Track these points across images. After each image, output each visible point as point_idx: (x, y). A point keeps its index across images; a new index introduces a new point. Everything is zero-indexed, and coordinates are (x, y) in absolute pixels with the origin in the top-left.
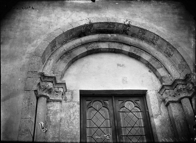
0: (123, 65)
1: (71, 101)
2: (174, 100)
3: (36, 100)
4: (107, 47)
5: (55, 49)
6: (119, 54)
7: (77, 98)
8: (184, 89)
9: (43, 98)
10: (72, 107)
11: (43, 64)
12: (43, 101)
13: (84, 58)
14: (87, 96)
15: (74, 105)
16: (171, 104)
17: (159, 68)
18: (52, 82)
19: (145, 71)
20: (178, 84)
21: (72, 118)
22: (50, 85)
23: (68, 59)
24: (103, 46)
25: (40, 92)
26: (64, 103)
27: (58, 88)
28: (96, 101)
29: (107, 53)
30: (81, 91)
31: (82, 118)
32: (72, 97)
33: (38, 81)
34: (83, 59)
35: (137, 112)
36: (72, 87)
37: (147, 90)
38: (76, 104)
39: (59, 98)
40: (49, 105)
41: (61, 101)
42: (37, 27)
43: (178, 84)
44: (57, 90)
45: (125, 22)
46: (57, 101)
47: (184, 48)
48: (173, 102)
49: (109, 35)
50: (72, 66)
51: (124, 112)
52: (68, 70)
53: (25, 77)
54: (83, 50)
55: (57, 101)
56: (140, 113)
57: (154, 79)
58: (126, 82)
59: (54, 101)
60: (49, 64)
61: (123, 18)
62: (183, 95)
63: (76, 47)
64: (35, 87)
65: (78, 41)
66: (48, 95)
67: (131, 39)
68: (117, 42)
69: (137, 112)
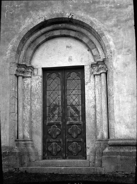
0: (70, 47)
1: (37, 75)
2: (98, 74)
3: (17, 79)
4: (60, 34)
5: (25, 42)
7: (40, 73)
8: (102, 68)
9: (20, 77)
10: (38, 79)
11: (18, 54)
12: (20, 78)
15: (38, 78)
16: (102, 74)
17: (93, 49)
18: (24, 67)
19: (85, 50)
21: (38, 86)
22: (23, 69)
24: (57, 33)
25: (18, 74)
26: (33, 77)
29: (60, 38)
30: (43, 68)
31: (44, 84)
32: (38, 73)
34: (44, 44)
35: (78, 79)
36: (37, 66)
37: (84, 66)
38: (40, 77)
40: (24, 79)
41: (30, 77)
42: (12, 28)
44: (28, 71)
45: (69, 16)
48: (97, 75)
49: (60, 25)
50: (37, 51)
52: (35, 53)
54: (43, 38)
57: (90, 56)
58: (71, 60)
59: (27, 77)
60: (22, 53)
61: (68, 12)
62: (101, 72)
63: (38, 37)
64: (15, 73)
65: (39, 33)
66: (23, 75)
67: (75, 27)
69: (78, 79)
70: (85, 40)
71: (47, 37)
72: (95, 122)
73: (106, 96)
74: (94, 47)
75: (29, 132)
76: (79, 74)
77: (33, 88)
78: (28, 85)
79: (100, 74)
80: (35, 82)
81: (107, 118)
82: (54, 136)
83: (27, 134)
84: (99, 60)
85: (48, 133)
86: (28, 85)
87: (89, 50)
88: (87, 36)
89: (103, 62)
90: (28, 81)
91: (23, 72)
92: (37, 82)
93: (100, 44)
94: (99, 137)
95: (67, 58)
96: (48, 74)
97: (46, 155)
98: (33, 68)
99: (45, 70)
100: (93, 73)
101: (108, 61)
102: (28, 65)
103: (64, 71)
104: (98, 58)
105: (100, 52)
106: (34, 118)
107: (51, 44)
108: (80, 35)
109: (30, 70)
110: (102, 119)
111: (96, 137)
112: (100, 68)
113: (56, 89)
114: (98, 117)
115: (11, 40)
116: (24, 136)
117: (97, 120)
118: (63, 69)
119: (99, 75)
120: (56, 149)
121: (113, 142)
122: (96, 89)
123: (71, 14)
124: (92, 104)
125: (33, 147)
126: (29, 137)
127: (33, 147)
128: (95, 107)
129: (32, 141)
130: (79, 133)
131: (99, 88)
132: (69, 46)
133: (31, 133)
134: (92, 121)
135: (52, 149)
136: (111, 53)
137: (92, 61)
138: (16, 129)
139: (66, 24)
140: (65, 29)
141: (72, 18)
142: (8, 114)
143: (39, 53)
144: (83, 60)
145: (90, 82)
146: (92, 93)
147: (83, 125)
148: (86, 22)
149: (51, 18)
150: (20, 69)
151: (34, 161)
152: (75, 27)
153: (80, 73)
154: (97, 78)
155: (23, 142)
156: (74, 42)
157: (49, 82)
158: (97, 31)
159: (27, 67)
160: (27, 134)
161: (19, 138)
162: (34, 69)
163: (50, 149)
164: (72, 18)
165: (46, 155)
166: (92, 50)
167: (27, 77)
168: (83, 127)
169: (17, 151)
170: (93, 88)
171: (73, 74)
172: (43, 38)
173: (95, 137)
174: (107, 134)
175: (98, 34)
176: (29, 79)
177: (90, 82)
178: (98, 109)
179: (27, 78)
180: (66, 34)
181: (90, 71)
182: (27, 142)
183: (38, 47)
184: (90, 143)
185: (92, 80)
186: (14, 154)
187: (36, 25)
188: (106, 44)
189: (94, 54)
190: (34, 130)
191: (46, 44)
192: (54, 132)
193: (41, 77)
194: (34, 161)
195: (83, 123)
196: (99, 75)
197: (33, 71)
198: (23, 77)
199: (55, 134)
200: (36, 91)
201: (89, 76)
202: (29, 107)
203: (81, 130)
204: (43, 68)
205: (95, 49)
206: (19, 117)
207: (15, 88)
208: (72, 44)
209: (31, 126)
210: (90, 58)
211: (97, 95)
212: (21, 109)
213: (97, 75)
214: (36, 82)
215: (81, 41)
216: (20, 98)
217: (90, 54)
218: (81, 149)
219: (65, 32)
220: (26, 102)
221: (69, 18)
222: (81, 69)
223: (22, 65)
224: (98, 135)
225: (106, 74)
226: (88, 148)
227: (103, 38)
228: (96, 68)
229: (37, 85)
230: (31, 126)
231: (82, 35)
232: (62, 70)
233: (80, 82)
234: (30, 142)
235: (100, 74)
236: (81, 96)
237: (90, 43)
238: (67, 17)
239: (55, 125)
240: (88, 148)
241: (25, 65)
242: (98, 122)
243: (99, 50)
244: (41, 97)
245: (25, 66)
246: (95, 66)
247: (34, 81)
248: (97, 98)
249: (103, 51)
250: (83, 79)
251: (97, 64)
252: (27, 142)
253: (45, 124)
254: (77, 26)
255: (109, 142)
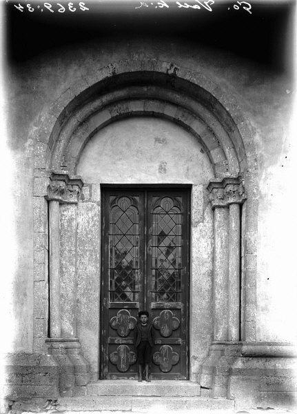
1: (89, 200)
2: (222, 204)
6: (156, 120)
7: (97, 195)
8: (234, 192)
10: (91, 210)
12: (55, 205)
13: (108, 127)
14: (108, 190)
16: (231, 207)
17: (213, 149)
18: (64, 181)
19: (196, 151)
20: (228, 184)
22: (62, 184)
23: (83, 133)
24: (136, 107)
26: (80, 204)
27: (72, 185)
28: (122, 197)
30: (102, 186)
32: (91, 195)
33: (47, 183)
34: (106, 129)
37: (191, 185)
38: (95, 205)
39: (73, 199)
41: (76, 204)
43: (228, 184)
44: (71, 189)
46: (72, 203)
47: (250, 124)
48: (220, 207)
50: (90, 144)
51: (159, 214)
53: (32, 177)
55: (72, 203)
56: (180, 216)
58: (165, 170)
59: (69, 203)
62: (231, 200)
64: (45, 192)
65: (97, 103)
66: (60, 198)
68: (157, 99)
70: (197, 126)
71: (115, 114)
72: (212, 307)
73: (238, 252)
74: (216, 144)
75: (72, 324)
76: (134, 200)
77: (80, 227)
78: (71, 220)
79: (228, 207)
80: (85, 216)
81: (238, 299)
82: (122, 332)
83: (68, 327)
84: (228, 174)
85: (110, 325)
86: (71, 220)
87: (205, 149)
88: (202, 120)
89: (237, 180)
90: (70, 211)
91: (62, 192)
92: (90, 215)
93: (231, 139)
94: (220, 336)
95: (157, 165)
96: (112, 198)
97: (106, 370)
98: (80, 182)
99: (107, 189)
100: (210, 202)
101: (248, 178)
102: (72, 177)
103: (148, 195)
104: (222, 171)
105: (228, 158)
106: (83, 294)
107: (121, 131)
108: (186, 114)
109: (76, 188)
110: (226, 299)
111: (212, 337)
112: (229, 193)
113: (128, 233)
114: (218, 296)
115: (36, 114)
116: (62, 332)
117: (217, 302)
118: (145, 188)
119: (223, 207)
120: (127, 359)
121: (251, 348)
122: (216, 236)
123: (172, 65)
124: (206, 268)
125: (81, 354)
126: (72, 333)
127: (81, 354)
128: (212, 274)
129: (78, 341)
130: (175, 325)
131: (224, 234)
132: (161, 139)
133: (76, 324)
134: (204, 303)
135: (120, 358)
136: (256, 160)
137: (209, 177)
138: (47, 317)
139: (159, 88)
140: (154, 98)
141: (174, 76)
142: (30, 284)
143: (94, 150)
144: (190, 173)
145: (203, 222)
146: (206, 244)
147: (185, 311)
148: (206, 85)
149: (127, 71)
150: (54, 184)
151: (86, 383)
152: (178, 98)
153: (180, 199)
154: (219, 214)
155: (62, 345)
156: (172, 129)
157: (111, 213)
158: (228, 109)
159: (69, 180)
160: (68, 327)
161: (52, 335)
162: (83, 184)
163: (114, 359)
164: (174, 76)
165: (106, 370)
166: (211, 152)
167: (69, 203)
168: (185, 315)
169: (53, 364)
170: (209, 234)
171: (166, 203)
172: (105, 116)
173: (209, 336)
174: (238, 332)
175: (231, 117)
176: (72, 209)
177: (203, 222)
178: (219, 279)
179: (69, 207)
180: (156, 110)
181: (204, 197)
182: (69, 344)
183: (91, 137)
184: (200, 349)
185: (208, 218)
186: (47, 371)
187: (94, 83)
188: (246, 140)
189: (215, 161)
190: (83, 320)
191: (110, 131)
192: (123, 324)
193: (98, 205)
194: (86, 383)
195: (185, 307)
196: (223, 207)
197: (81, 189)
198: (61, 203)
199: (126, 327)
200: (87, 234)
201: (201, 208)
202: (72, 269)
203: (180, 319)
204: (102, 186)
205: (216, 150)
206: (53, 292)
207: (45, 227)
208: (166, 133)
209: (76, 310)
210: (205, 169)
211: (218, 250)
212: (56, 273)
213: (220, 207)
214: (87, 214)
215: (187, 129)
216: (55, 250)
217: (206, 162)
218: (180, 358)
219: (153, 107)
220: (67, 259)
221: (167, 74)
222: (184, 191)
223: (59, 175)
224: (217, 332)
225: (241, 205)
226: (195, 358)
227: (241, 125)
228: (219, 193)
229: (88, 222)
230: (76, 310)
231: (190, 116)
232: (144, 191)
233: (180, 219)
234: (76, 344)
235: (228, 207)
236: (182, 250)
237: (209, 135)
238: (164, 71)
239: (127, 309)
240: (195, 358)
241: (67, 176)
242: (217, 306)
243: (227, 153)
244: (98, 248)
245: (66, 179)
246: (217, 187)
247: (83, 212)
248: (218, 256)
249: (237, 154)
250: (187, 213)
251: (223, 184)
252: (69, 344)
253: (104, 307)
254: (181, 93)
255: (245, 348)
